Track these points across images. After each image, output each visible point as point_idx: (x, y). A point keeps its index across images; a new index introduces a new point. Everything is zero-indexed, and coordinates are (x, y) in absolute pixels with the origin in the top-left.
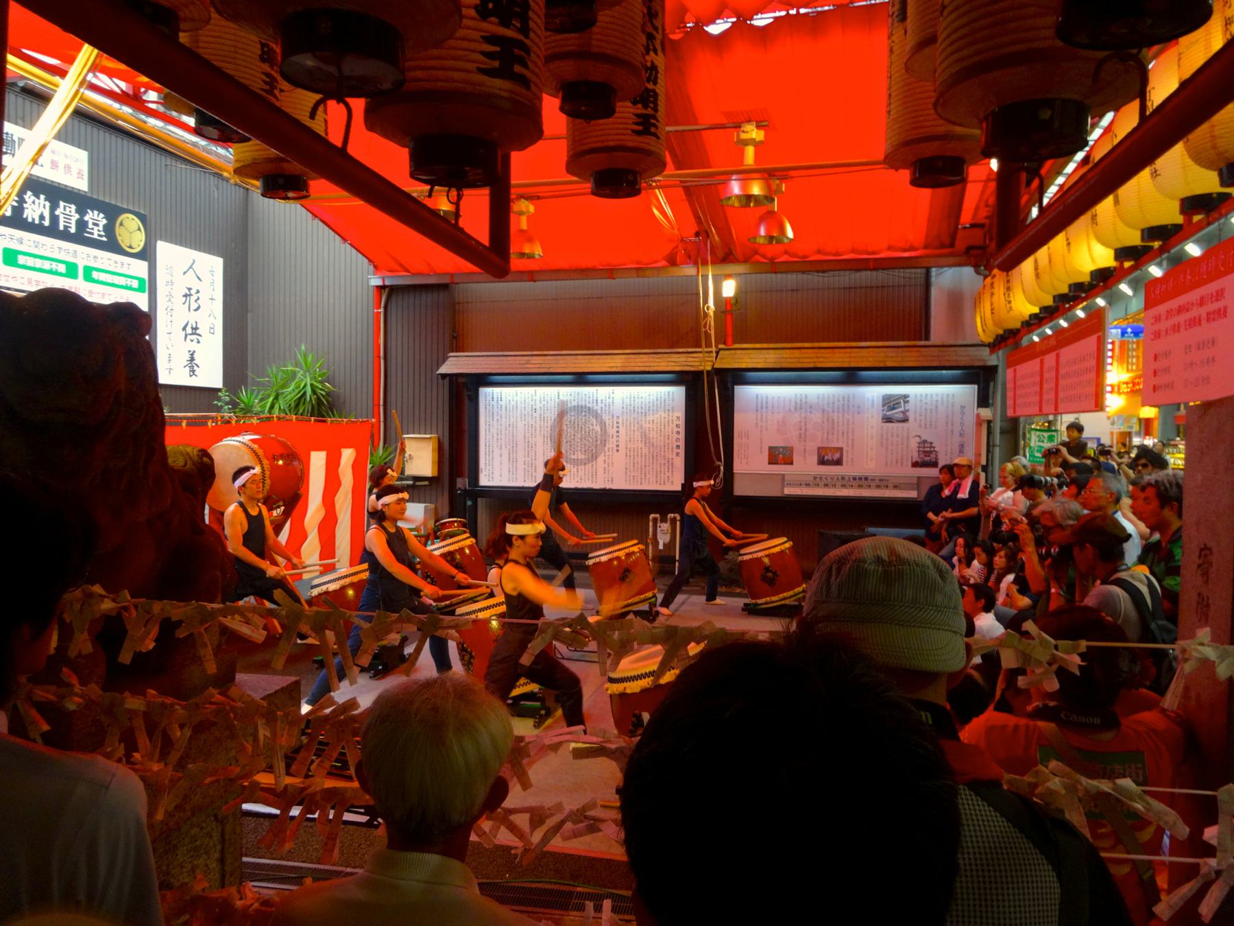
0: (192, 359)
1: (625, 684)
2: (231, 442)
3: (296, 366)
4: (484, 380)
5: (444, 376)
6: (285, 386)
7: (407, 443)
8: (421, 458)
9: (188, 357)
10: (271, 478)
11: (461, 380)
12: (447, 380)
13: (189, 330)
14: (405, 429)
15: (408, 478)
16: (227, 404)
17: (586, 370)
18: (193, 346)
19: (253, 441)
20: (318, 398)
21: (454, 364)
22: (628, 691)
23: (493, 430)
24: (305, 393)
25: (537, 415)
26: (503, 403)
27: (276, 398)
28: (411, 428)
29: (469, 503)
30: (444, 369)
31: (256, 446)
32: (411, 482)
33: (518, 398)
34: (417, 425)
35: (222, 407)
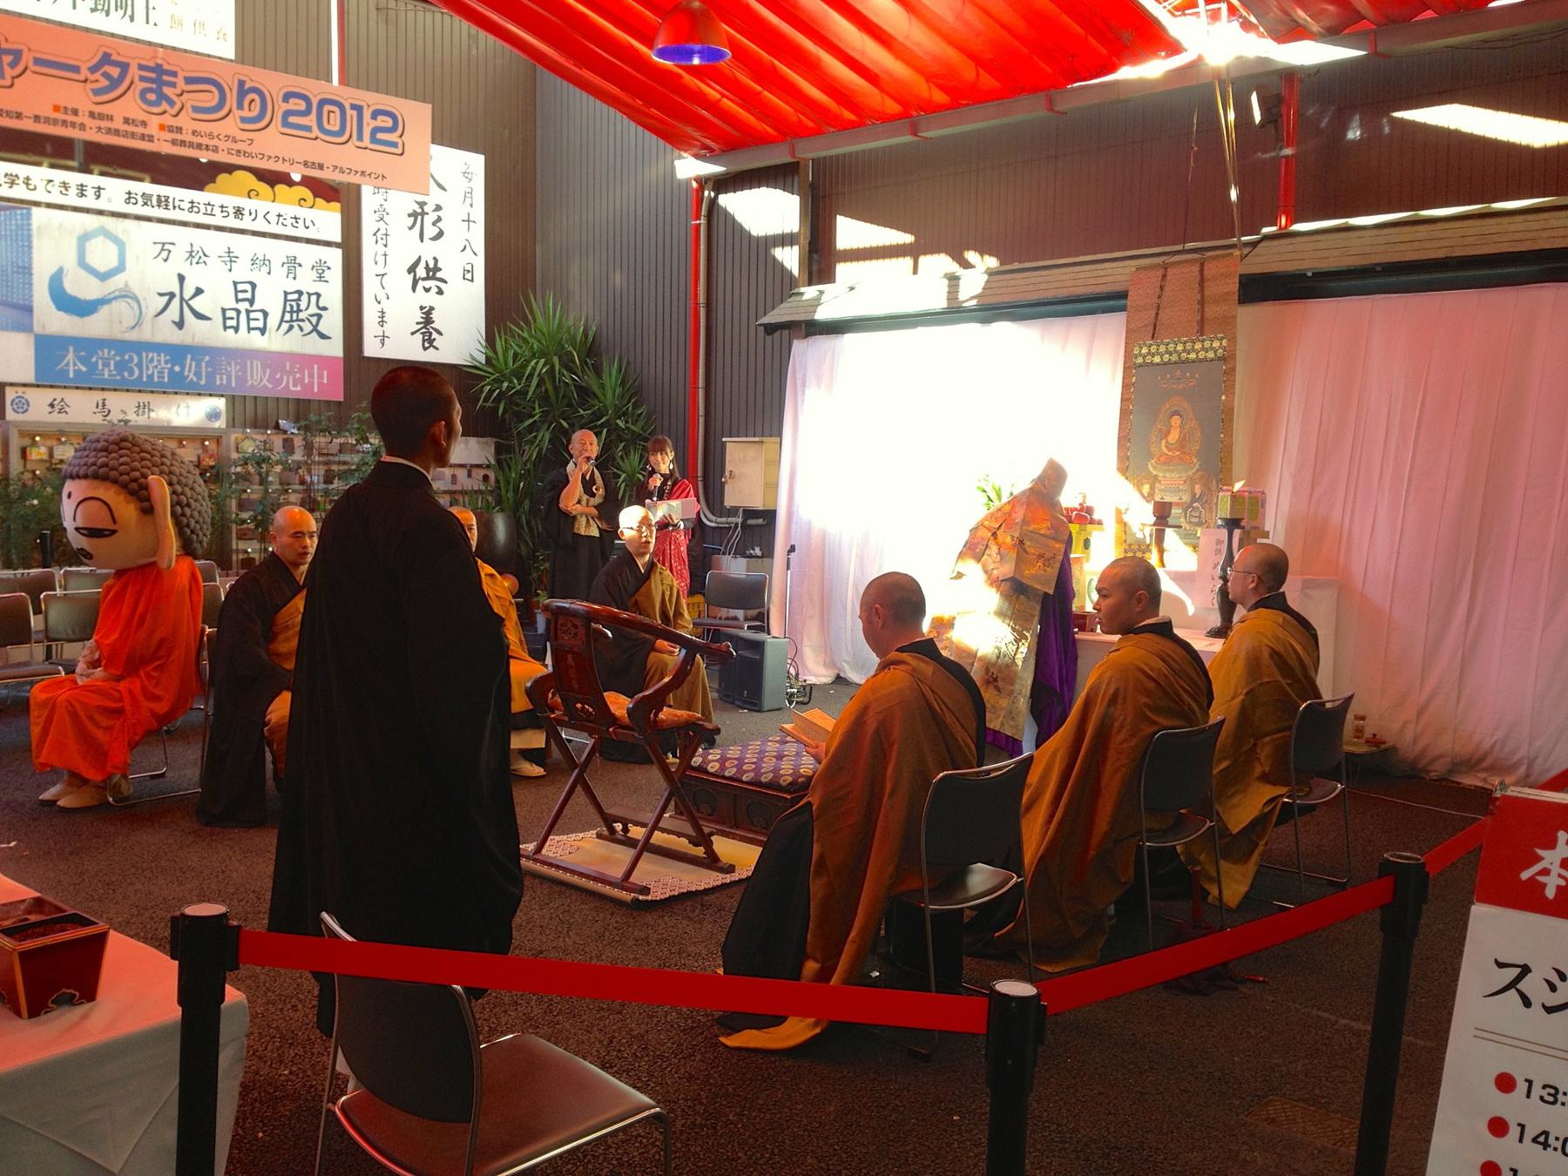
9: (419, 316)
13: (421, 272)
15: (733, 511)
18: (430, 299)
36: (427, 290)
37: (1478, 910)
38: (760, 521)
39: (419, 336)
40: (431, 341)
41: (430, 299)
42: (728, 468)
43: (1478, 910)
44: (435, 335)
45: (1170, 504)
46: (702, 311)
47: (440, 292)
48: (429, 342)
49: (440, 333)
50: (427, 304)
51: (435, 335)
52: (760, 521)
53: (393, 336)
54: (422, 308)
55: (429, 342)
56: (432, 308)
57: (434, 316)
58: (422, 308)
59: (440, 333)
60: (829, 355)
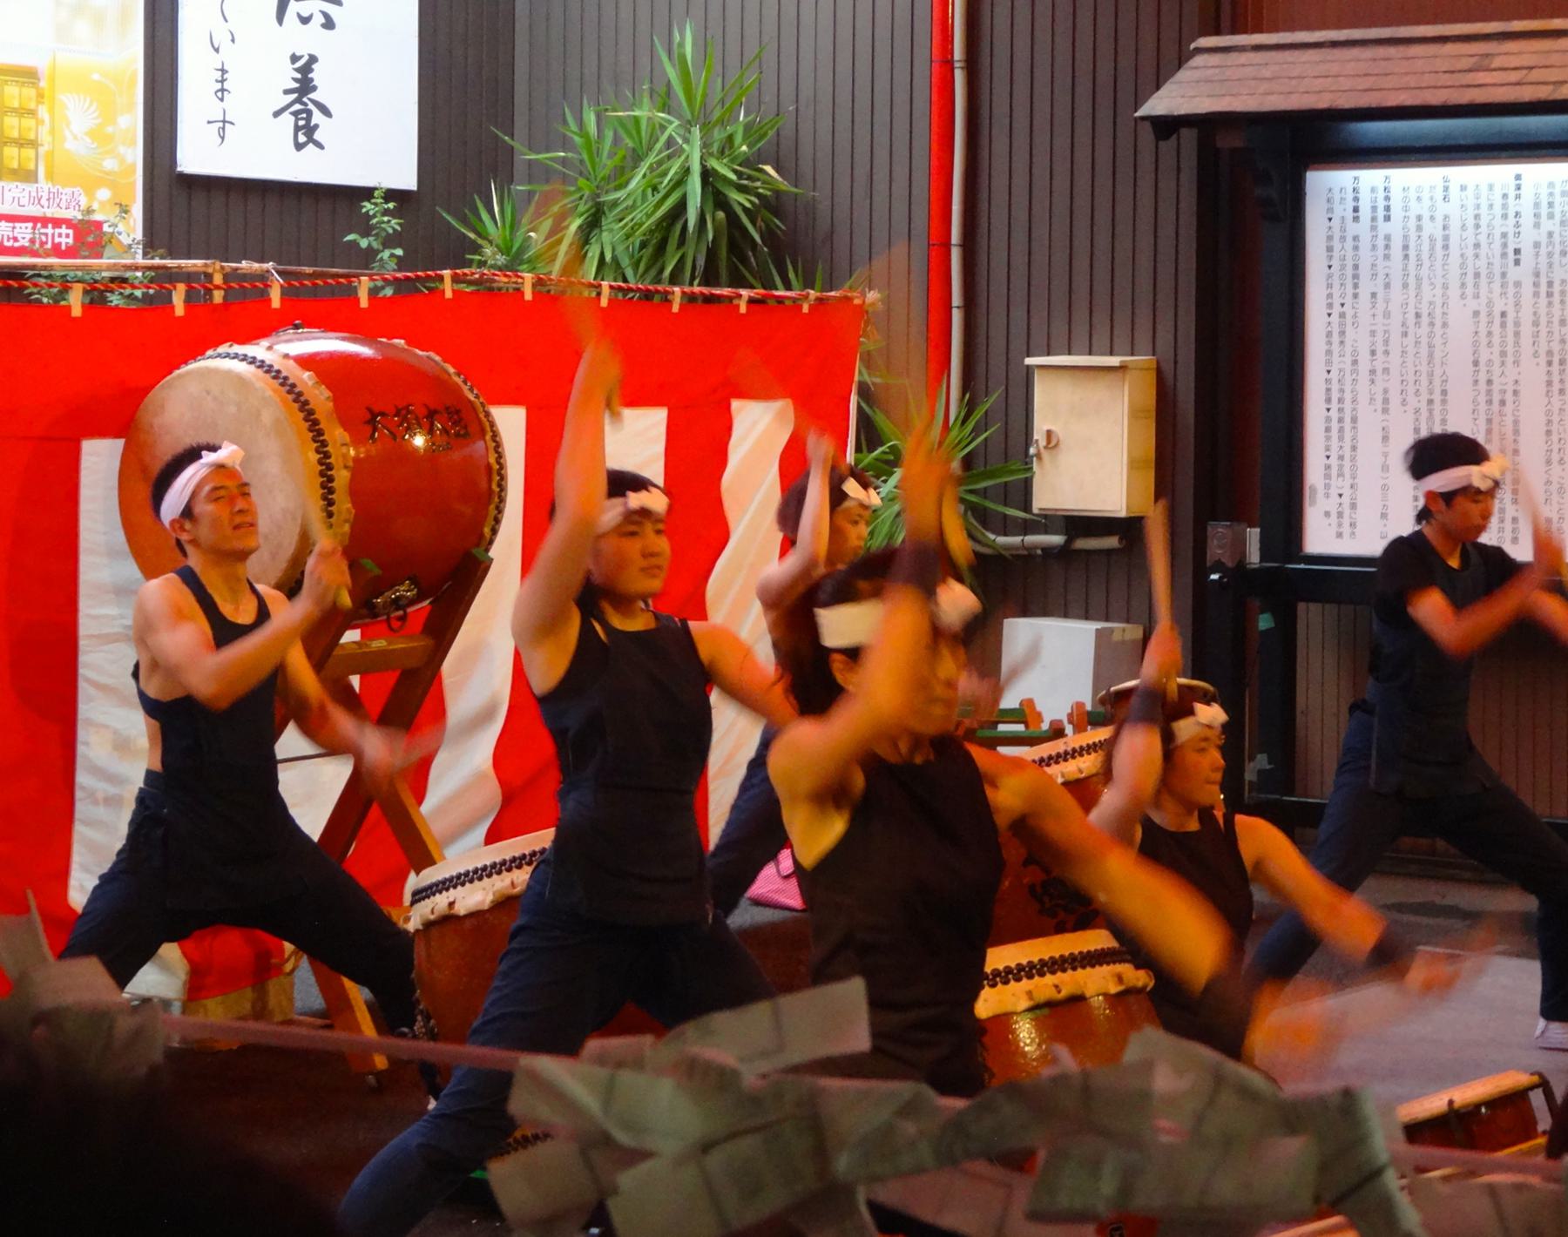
0: (305, 86)
1: (452, 894)
2: (227, 363)
3: (665, 108)
4: (1323, 137)
5: (1166, 126)
6: (619, 176)
7: (1043, 393)
8: (1091, 446)
9: (287, 77)
10: (354, 492)
11: (1228, 141)
12: (1189, 136)
14: (1039, 337)
15: (1048, 521)
16: (389, 242)
17: (1346, 102)
18: (309, 40)
19: (306, 362)
20: (732, 218)
21: (1216, 80)
22: (461, 909)
23: (1359, 339)
24: (681, 206)
25: (1523, 273)
26: (1394, 228)
27: (593, 223)
28: (1081, 330)
29: (1265, 622)
30: (1173, 98)
31: (307, 377)
32: (1057, 539)
33: (1452, 208)
34: (1084, 320)
35: (371, 253)
36: (305, 20)
37: (736, 404)
38: (1112, 542)
39: (288, 120)
40: (310, 130)
41: (309, 40)
42: (1040, 426)
43: (736, 404)
44: (317, 117)
45: (791, 847)
46: (959, 77)
47: (329, 24)
48: (306, 133)
49: (326, 112)
50: (304, 51)
51: (317, 117)
52: (1112, 542)
53: (237, 136)
54: (294, 58)
55: (306, 133)
56: (313, 59)
57: (317, 75)
58: (294, 58)
59: (326, 112)
60: (1343, 736)
